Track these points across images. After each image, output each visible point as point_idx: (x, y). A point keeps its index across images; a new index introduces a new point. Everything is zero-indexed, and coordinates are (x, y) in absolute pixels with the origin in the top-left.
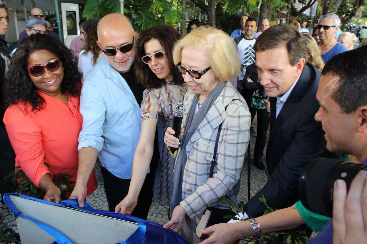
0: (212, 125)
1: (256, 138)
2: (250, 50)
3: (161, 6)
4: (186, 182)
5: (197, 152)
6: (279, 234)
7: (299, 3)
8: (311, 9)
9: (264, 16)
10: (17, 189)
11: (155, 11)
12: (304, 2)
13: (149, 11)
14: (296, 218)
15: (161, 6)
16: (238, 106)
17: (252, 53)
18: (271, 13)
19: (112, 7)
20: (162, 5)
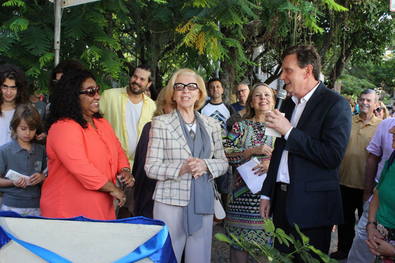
0: (184, 191)
1: (272, 221)
2: (216, 117)
3: (99, 53)
4: (187, 190)
5: (179, 192)
6: (301, 38)
7: (263, 73)
8: (279, 82)
9: (225, 82)
10: (33, 85)
11: (90, 57)
12: (269, 71)
13: (81, 57)
14: (387, 248)
15: (99, 53)
16: (223, 164)
17: (219, 116)
18: (234, 78)
19: (32, 48)
20: (98, 52)
